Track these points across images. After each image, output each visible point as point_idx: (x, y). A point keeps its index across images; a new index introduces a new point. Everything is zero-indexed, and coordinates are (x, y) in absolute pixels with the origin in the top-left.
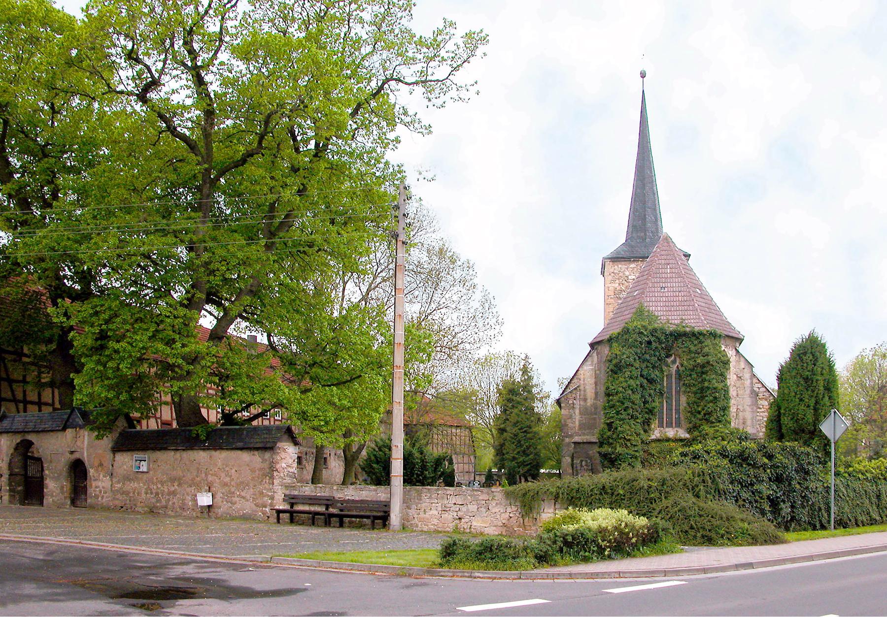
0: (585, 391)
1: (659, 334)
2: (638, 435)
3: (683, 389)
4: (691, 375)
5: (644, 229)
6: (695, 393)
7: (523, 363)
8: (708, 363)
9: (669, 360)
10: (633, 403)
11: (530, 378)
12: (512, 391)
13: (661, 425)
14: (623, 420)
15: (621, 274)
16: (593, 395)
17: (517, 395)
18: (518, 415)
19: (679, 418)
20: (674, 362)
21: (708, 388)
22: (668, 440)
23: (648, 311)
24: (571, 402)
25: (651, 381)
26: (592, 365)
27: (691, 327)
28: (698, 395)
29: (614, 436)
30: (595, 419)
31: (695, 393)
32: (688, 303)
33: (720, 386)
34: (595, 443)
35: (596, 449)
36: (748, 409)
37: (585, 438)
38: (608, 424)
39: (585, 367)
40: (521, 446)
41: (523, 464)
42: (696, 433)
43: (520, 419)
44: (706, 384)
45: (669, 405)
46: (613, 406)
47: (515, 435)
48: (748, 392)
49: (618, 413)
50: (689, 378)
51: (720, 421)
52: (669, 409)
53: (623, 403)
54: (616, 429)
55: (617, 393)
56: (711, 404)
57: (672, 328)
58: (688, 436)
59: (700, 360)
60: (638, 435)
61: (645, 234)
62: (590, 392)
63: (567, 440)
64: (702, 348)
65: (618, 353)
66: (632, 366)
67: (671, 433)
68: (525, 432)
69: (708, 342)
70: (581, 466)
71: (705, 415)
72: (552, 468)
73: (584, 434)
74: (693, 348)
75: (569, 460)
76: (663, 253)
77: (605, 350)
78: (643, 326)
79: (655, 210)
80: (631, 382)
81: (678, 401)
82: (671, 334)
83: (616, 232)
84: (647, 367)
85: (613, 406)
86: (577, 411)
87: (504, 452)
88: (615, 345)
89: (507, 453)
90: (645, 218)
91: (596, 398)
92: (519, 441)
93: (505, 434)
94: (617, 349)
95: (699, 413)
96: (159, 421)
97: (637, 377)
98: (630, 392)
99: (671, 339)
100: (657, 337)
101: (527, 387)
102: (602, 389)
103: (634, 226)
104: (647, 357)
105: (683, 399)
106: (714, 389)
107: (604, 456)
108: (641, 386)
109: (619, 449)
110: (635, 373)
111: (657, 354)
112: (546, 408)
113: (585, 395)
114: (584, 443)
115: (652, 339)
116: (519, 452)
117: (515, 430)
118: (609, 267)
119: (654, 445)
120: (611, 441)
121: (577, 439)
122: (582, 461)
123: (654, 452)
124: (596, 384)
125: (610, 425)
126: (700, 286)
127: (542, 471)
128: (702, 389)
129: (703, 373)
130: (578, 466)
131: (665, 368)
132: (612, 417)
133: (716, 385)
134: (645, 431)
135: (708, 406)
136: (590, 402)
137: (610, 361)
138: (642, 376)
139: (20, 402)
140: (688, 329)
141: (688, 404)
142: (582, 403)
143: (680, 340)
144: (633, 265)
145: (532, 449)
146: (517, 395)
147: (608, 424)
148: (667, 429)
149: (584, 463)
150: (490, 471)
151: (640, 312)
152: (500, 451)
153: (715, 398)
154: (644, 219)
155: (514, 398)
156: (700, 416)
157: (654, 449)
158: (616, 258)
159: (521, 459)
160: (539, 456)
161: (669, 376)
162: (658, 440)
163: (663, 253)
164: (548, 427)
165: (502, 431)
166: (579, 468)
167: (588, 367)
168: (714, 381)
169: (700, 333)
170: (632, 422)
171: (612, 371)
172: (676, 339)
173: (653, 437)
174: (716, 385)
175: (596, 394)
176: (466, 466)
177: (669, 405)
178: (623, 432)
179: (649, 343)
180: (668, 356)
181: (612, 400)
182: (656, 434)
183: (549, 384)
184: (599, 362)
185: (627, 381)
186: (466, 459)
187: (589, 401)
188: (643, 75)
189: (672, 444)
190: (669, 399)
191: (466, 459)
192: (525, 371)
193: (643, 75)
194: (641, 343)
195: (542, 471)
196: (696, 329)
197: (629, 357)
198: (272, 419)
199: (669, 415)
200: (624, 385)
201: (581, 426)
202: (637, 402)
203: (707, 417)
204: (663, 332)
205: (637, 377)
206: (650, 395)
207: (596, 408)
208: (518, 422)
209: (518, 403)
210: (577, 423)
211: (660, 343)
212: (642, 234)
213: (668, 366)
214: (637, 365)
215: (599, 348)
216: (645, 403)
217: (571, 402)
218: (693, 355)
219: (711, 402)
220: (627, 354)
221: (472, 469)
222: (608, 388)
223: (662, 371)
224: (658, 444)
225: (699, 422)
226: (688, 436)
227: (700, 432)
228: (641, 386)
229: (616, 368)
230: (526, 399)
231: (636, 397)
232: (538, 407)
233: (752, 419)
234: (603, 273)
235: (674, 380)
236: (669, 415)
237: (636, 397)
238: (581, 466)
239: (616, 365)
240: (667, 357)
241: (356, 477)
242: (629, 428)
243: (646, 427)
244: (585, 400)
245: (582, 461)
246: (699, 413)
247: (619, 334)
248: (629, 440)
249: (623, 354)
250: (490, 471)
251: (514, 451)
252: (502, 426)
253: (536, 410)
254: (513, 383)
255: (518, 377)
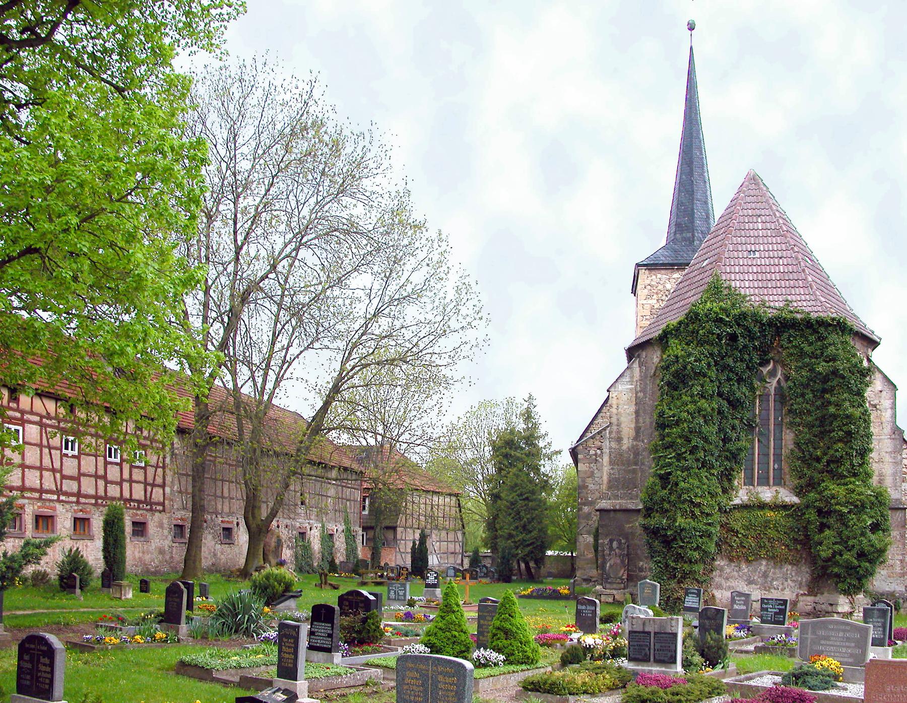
0: (619, 425)
1: (749, 323)
2: (713, 495)
3: (787, 420)
4: (803, 395)
5: (691, 227)
6: (810, 426)
7: (526, 405)
8: (835, 373)
9: (765, 370)
10: (706, 439)
11: (535, 426)
12: (510, 444)
13: (749, 481)
14: (688, 469)
15: (660, 287)
16: (632, 433)
17: (516, 449)
18: (517, 476)
19: (780, 469)
20: (773, 374)
21: (835, 417)
22: (762, 506)
23: (729, 288)
24: (592, 452)
25: (735, 404)
26: (631, 382)
27: (803, 312)
28: (816, 430)
29: (673, 498)
30: (634, 471)
31: (810, 426)
32: (795, 276)
33: (857, 413)
34: (639, 510)
35: (641, 520)
36: (887, 458)
37: (618, 503)
38: (661, 477)
39: (620, 387)
40: (520, 519)
41: (523, 544)
42: (812, 495)
43: (519, 482)
44: (832, 409)
45: (764, 446)
46: (670, 446)
47: (512, 504)
48: (887, 429)
49: (679, 457)
50: (800, 400)
51: (855, 475)
52: (765, 455)
53: (689, 441)
54: (677, 484)
55: (677, 423)
56: (840, 445)
57: (771, 313)
58: (796, 500)
59: (822, 367)
60: (713, 495)
61: (693, 236)
62: (628, 428)
63: (586, 509)
64: (824, 348)
65: (680, 353)
66: (705, 376)
67: (767, 494)
68: (527, 499)
69: (833, 337)
70: (611, 548)
71: (828, 462)
72: (563, 549)
73: (616, 497)
74: (807, 348)
75: (590, 539)
76: (748, 199)
77: (655, 357)
78: (721, 309)
79: (706, 203)
80: (703, 403)
81: (779, 439)
82: (771, 323)
83: (655, 238)
84: (729, 379)
85: (670, 446)
86: (606, 459)
87: (497, 526)
88: (673, 342)
89: (501, 529)
90: (693, 213)
91: (636, 438)
92: (518, 513)
93: (499, 502)
94: (676, 348)
95: (818, 460)
96: (58, 475)
97: (712, 396)
98: (702, 421)
99: (770, 332)
100: (747, 329)
101: (531, 437)
102: (648, 420)
103: (678, 225)
104: (730, 361)
105: (789, 437)
106: (848, 417)
107: (654, 532)
108: (720, 412)
109: (680, 521)
110: (710, 388)
111: (746, 357)
112: (558, 466)
113: (619, 432)
114: (615, 511)
115: (739, 331)
116: (517, 527)
117: (513, 496)
118: (645, 278)
119: (737, 514)
120: (666, 506)
121: (604, 504)
122: (611, 541)
123: (737, 526)
124: (637, 413)
125: (664, 479)
126: (808, 255)
127: (549, 553)
128: (822, 420)
129: (825, 391)
130: (606, 548)
131: (757, 384)
132: (670, 464)
133: (851, 410)
134: (725, 491)
135: (836, 447)
136: (626, 443)
137: (667, 368)
138: (720, 395)
139: (149, 484)
140: (799, 316)
141: (797, 444)
142: (614, 445)
143: (786, 335)
144: (676, 275)
145: (535, 524)
146: (516, 451)
147: (661, 477)
148: (760, 489)
149: (615, 544)
150: (476, 552)
151: (715, 290)
152: (492, 525)
153: (849, 433)
154: (691, 215)
155: (513, 453)
156: (820, 466)
157: (738, 522)
158: (652, 266)
159: (520, 537)
160: (545, 533)
161: (764, 397)
162: (744, 507)
163: (748, 199)
164: (558, 497)
165: (496, 497)
166: (607, 552)
167: (625, 387)
168: (847, 404)
169: (821, 323)
170: (704, 473)
171: (669, 384)
172: (779, 332)
173: (737, 501)
174: (851, 410)
175: (638, 430)
176: (451, 546)
177: (764, 446)
178: (688, 491)
179: (733, 338)
180: (765, 363)
181: (668, 435)
182: (741, 496)
183: (559, 433)
184: (643, 379)
185: (695, 402)
186: (451, 536)
187: (625, 441)
188: (691, 28)
189: (770, 514)
190: (764, 436)
191: (451, 536)
192: (528, 416)
193: (691, 28)
194: (719, 337)
195: (549, 553)
196: (814, 316)
197: (700, 361)
198: (126, 467)
199: (764, 464)
200: (691, 407)
201: (613, 483)
202: (713, 438)
203: (833, 468)
204: (756, 318)
205: (712, 396)
206: (733, 428)
207: (637, 454)
208: (516, 485)
209: (518, 459)
210: (605, 478)
211: (752, 338)
212: (689, 235)
213: (762, 380)
214: (713, 374)
215: (644, 354)
216: (726, 440)
217: (592, 452)
218: (807, 360)
219: (840, 440)
220: (694, 355)
221: (458, 549)
222: (661, 415)
223: (752, 389)
224: (745, 513)
225: (817, 475)
226: (796, 500)
227: (820, 493)
228: (719, 413)
229: (676, 380)
230: (528, 455)
231: (711, 430)
232: (546, 467)
233: (894, 474)
234: (634, 291)
235: (772, 404)
236: (764, 464)
237: (711, 430)
238: (611, 548)
239: (676, 375)
240: (761, 364)
241: (265, 560)
242: (697, 484)
243: (726, 484)
244: (619, 440)
245: (611, 541)
246: (818, 460)
247: (680, 323)
248: (698, 505)
249: (689, 355)
250: (476, 552)
251: (510, 524)
252: (495, 491)
253: (542, 469)
254: (512, 432)
255: (521, 426)
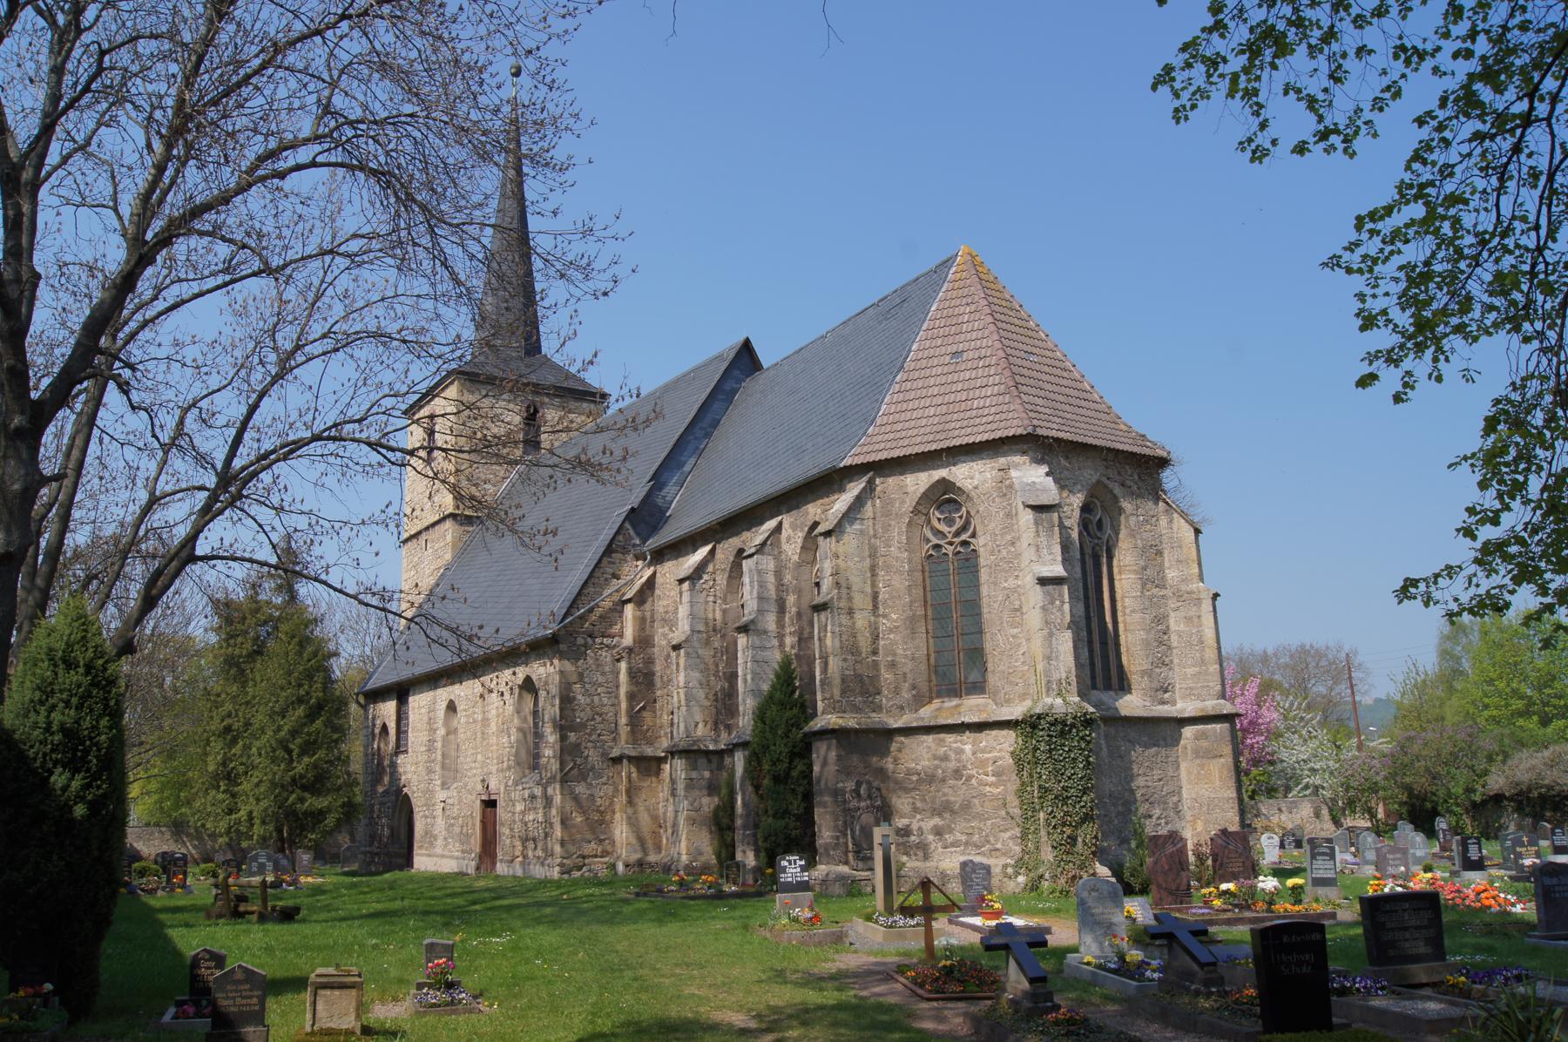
24: (580, 641)
245: (859, 784)
